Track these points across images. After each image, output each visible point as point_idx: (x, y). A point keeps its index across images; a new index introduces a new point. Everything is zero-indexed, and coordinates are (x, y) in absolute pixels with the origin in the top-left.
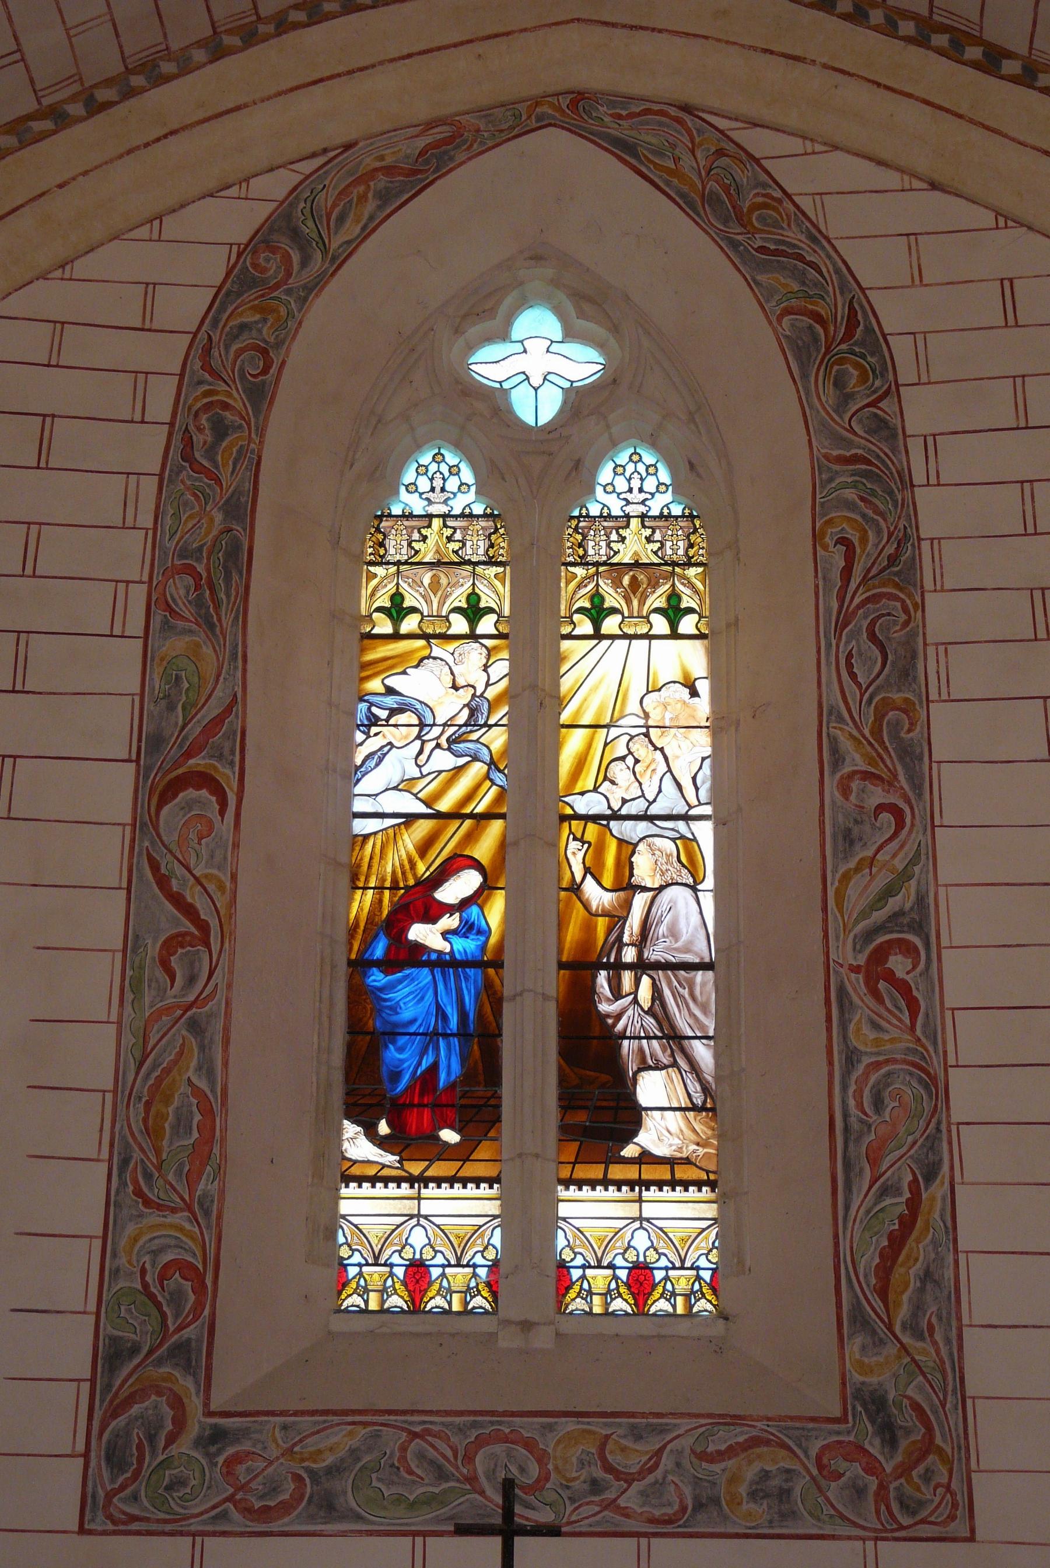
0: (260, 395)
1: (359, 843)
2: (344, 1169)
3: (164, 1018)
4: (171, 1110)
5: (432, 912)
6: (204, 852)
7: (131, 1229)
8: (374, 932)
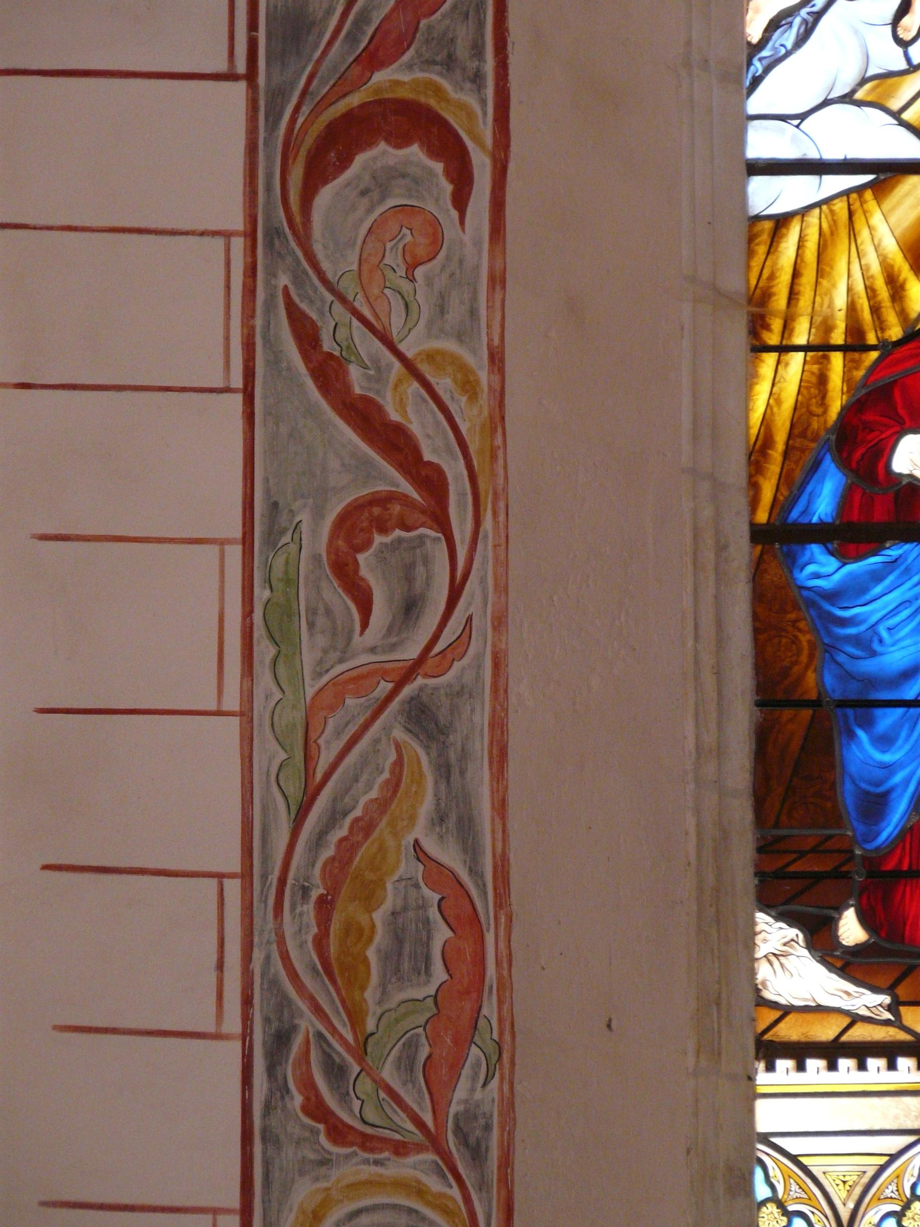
1: (765, 237)
2: (761, 1027)
3: (350, 701)
4: (379, 917)
6: (423, 299)
7: (304, 1192)
8: (808, 458)
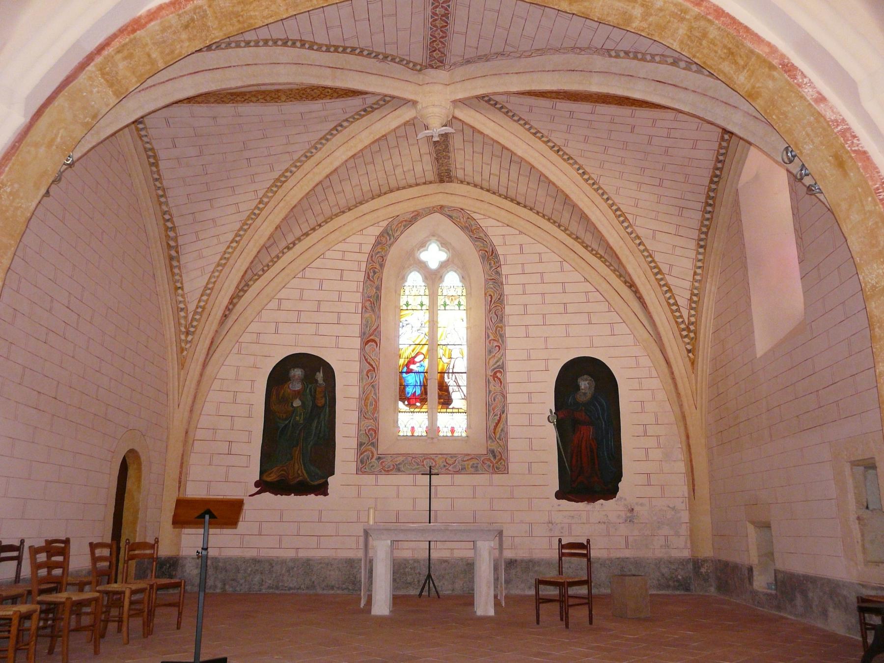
0: (382, 266)
5: (414, 363)
